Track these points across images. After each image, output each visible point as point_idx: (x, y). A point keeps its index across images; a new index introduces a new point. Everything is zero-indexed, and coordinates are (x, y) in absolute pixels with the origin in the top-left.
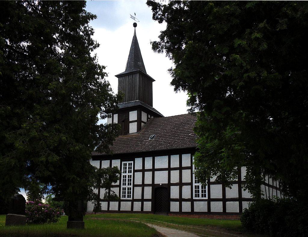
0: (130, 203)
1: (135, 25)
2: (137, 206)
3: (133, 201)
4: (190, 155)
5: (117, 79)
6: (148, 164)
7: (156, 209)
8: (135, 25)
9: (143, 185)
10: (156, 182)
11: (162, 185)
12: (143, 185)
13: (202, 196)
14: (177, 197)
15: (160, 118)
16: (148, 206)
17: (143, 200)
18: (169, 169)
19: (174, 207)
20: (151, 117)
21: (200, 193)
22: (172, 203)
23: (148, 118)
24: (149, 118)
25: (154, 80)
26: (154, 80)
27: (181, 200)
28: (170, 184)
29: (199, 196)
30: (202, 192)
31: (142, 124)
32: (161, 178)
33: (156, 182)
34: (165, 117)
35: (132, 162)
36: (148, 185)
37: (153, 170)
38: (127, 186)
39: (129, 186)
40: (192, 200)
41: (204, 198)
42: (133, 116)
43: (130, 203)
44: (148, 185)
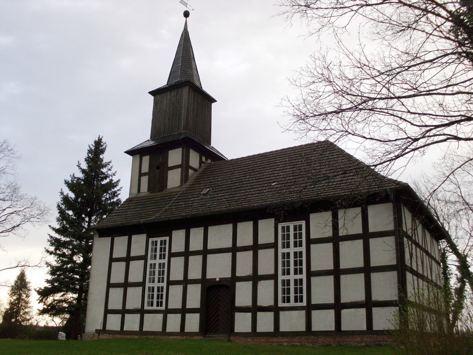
0: (160, 317)
1: (186, 14)
2: (174, 323)
3: (310, 308)
4: (272, 221)
5: (152, 98)
6: (196, 243)
7: (207, 327)
8: (186, 14)
9: (186, 282)
10: (209, 276)
11: (219, 281)
12: (186, 282)
13: (296, 301)
14: (249, 303)
15: (218, 163)
16: (193, 323)
17: (184, 311)
18: (234, 250)
19: (242, 323)
20: (206, 160)
21: (292, 295)
22: (238, 316)
23: (201, 162)
24: (203, 163)
25: (214, 101)
26: (214, 101)
27: (255, 309)
28: (234, 279)
29: (289, 301)
30: (296, 292)
31: (191, 171)
32: (219, 268)
33: (209, 276)
34: (229, 158)
35: (303, 223)
36: (195, 282)
37: (205, 252)
38: (156, 285)
39: (161, 285)
40: (275, 310)
41: (299, 304)
42: (175, 157)
43: (160, 317)
44: (195, 282)
